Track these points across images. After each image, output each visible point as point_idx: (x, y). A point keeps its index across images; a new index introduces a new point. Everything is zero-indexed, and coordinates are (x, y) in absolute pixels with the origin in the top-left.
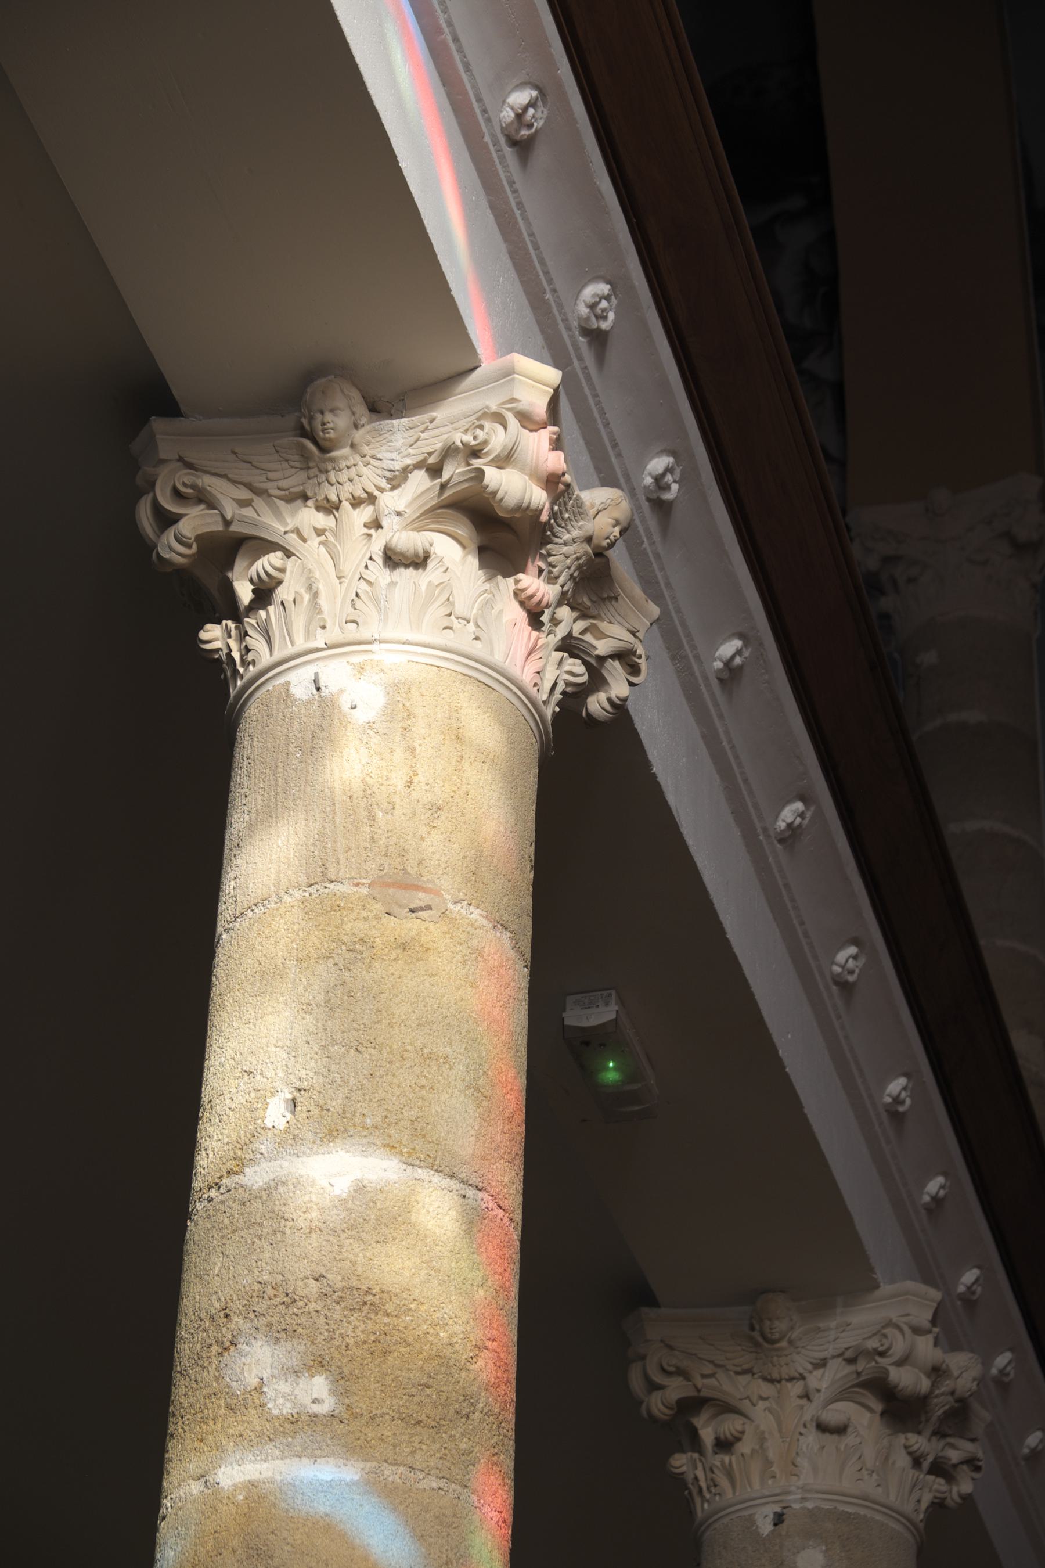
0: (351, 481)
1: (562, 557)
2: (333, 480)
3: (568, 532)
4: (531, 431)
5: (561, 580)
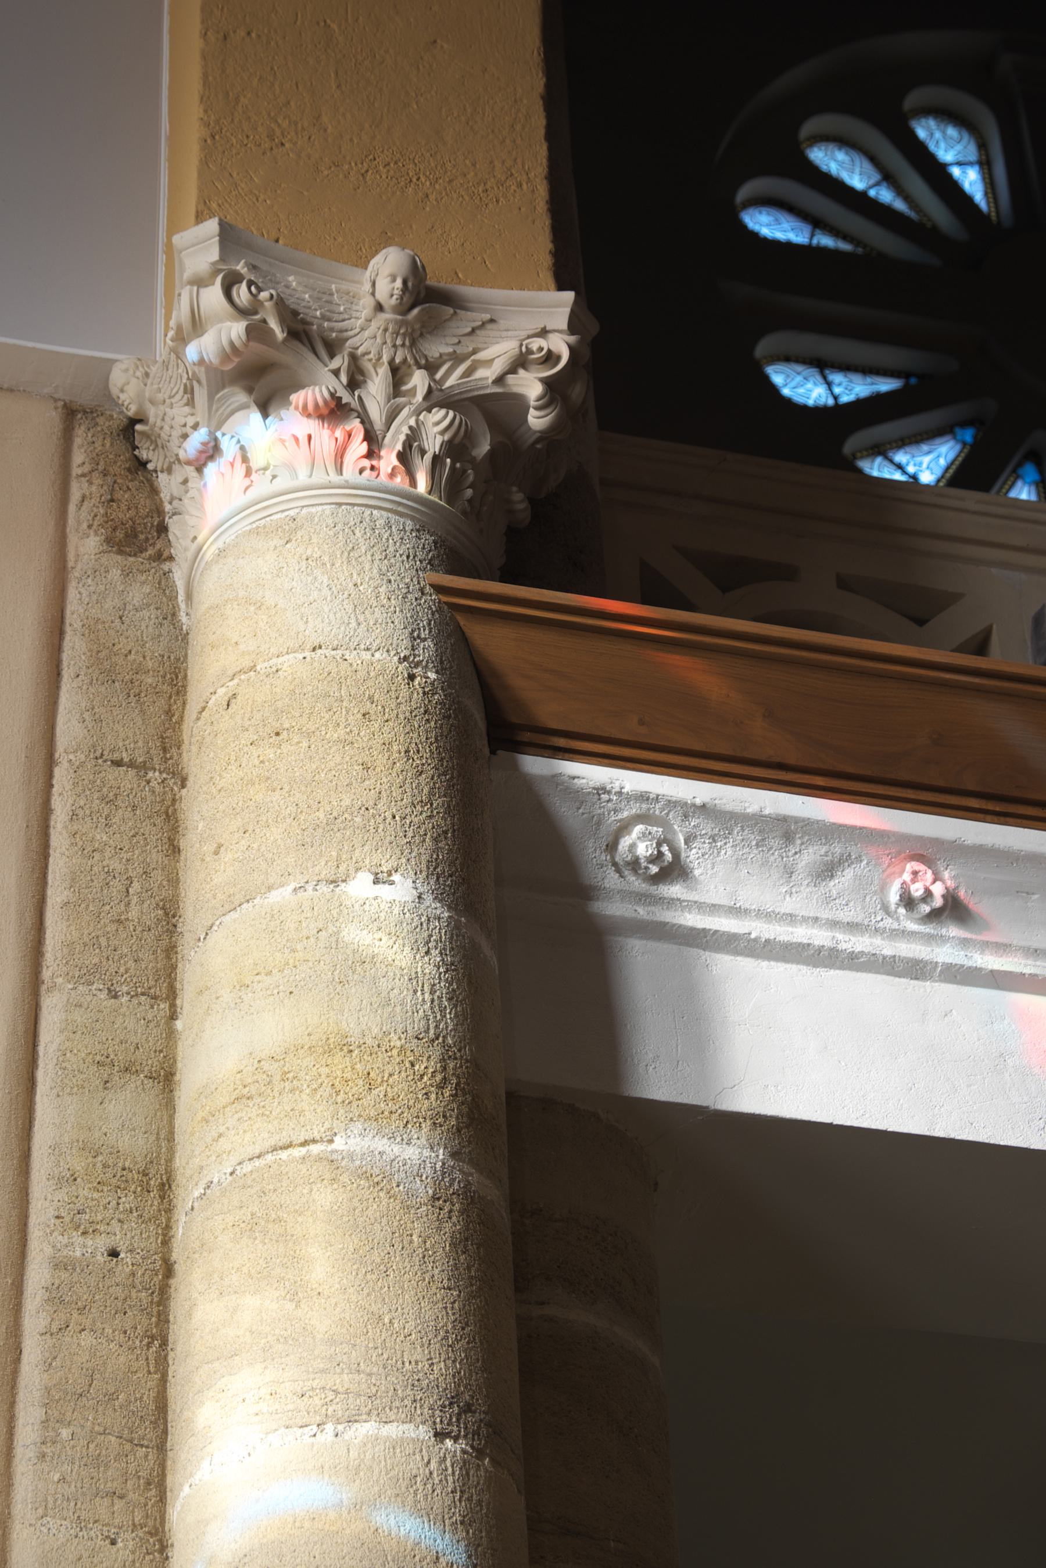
3: (357, 318)
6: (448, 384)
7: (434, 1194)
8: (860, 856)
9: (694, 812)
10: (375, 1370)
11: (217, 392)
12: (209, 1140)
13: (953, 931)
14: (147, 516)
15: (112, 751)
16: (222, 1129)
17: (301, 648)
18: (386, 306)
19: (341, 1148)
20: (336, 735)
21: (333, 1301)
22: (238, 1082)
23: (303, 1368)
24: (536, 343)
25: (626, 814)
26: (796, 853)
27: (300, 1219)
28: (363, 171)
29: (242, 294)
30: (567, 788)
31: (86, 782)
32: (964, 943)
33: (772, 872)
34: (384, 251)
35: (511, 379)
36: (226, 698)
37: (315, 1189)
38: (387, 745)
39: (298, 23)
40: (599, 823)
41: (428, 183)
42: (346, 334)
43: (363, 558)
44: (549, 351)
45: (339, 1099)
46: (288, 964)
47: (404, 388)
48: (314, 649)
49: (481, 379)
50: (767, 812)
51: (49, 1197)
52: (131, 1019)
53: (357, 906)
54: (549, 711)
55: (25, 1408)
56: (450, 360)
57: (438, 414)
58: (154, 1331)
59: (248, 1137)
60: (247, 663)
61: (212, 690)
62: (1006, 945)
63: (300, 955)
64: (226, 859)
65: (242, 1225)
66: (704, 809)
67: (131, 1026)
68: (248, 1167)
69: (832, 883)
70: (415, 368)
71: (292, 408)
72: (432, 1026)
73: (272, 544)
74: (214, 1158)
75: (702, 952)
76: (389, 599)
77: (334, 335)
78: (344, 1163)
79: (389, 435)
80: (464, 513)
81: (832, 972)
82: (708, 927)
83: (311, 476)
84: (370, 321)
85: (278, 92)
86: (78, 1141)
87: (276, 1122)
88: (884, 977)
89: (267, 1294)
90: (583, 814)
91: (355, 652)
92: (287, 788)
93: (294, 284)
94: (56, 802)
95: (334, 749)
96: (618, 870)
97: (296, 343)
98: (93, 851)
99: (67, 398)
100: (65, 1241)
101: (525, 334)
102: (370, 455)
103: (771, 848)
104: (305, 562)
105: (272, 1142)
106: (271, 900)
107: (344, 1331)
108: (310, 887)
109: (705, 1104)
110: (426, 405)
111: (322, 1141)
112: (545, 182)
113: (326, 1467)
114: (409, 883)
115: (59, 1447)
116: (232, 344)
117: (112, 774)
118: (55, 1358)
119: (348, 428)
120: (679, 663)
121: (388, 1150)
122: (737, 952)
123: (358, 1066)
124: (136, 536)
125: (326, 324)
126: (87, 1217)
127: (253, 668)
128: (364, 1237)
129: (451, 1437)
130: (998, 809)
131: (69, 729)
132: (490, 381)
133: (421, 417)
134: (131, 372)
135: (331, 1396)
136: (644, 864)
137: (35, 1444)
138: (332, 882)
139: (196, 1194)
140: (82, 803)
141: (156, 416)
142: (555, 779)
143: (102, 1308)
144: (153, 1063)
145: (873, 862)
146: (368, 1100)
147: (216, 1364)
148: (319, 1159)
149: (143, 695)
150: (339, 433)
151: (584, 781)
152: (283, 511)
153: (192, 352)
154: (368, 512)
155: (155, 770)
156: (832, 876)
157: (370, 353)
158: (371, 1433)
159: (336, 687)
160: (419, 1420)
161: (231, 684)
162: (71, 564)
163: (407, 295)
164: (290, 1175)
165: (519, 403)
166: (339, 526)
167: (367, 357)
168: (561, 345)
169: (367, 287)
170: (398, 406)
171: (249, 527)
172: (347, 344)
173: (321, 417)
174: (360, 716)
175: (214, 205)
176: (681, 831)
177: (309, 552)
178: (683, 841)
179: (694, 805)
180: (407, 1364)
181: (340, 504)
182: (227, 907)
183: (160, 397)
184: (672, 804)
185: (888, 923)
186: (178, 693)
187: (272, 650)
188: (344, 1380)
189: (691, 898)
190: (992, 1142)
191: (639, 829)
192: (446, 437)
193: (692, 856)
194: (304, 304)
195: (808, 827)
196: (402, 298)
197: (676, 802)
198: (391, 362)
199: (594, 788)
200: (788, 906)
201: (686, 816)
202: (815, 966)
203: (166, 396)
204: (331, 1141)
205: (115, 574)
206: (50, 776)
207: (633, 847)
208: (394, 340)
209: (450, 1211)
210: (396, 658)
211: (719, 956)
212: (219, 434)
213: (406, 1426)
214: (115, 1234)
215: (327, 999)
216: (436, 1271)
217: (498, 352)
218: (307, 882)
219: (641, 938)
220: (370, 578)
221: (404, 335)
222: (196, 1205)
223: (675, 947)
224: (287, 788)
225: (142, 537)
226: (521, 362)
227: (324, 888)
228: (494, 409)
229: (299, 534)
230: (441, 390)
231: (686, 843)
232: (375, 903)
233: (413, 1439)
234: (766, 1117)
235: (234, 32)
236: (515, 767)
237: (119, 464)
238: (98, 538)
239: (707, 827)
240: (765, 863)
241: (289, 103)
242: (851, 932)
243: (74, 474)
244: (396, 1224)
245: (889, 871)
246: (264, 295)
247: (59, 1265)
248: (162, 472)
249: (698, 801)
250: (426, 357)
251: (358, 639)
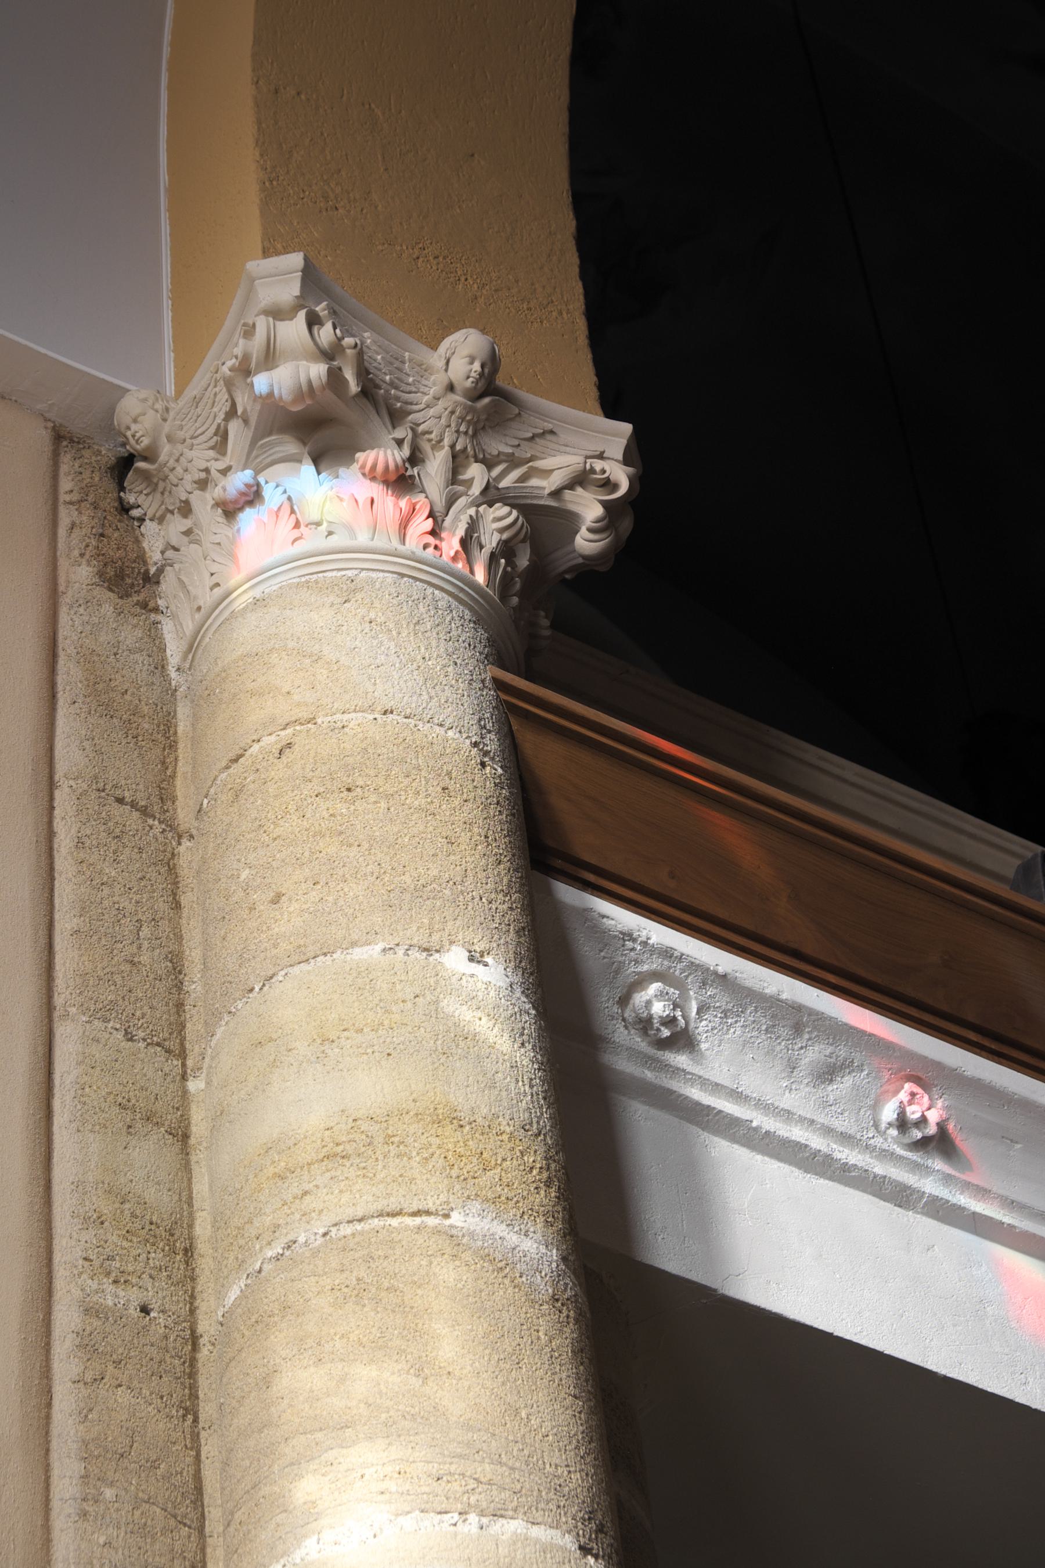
0: (186, 470)
1: (433, 421)
2: (175, 481)
3: (424, 394)
4: (291, 319)
5: (446, 442)
7: (554, 1295)
8: (862, 1065)
9: (713, 981)
10: (518, 1465)
11: (263, 437)
12: (289, 1198)
13: (938, 1164)
14: (135, 561)
15: (115, 786)
16: (307, 1187)
17: (371, 709)
18: (458, 387)
19: (460, 1224)
20: (417, 803)
21: (466, 1384)
22: (327, 1139)
23: (437, 1450)
24: (598, 465)
25: (646, 968)
26: (802, 1048)
27: (419, 1292)
28: (415, 256)
29: (326, 334)
30: (595, 926)
31: (90, 811)
32: (947, 1179)
33: (776, 1063)
34: (464, 331)
36: (279, 747)
37: (435, 1263)
38: (468, 824)
39: (345, 98)
40: (617, 972)
41: (475, 286)
42: (410, 407)
43: (429, 634)
45: (454, 1172)
46: (382, 1024)
47: (461, 477)
48: (385, 713)
49: (537, 488)
50: (784, 996)
51: (75, 1236)
52: (150, 1067)
53: (454, 980)
54: (585, 843)
55: (59, 1459)
56: (506, 461)
58: (188, 1403)
59: (345, 1198)
60: (305, 715)
61: (255, 737)
62: (985, 1190)
63: (396, 1017)
64: (291, 909)
65: (346, 1290)
66: (723, 979)
67: (150, 1074)
68: (347, 1230)
69: (830, 1088)
70: (473, 460)
71: (355, 466)
72: (535, 1120)
73: (332, 598)
74: (297, 1216)
75: (701, 1132)
76: (457, 681)
77: (399, 405)
78: (465, 1241)
81: (822, 1181)
82: (713, 1105)
83: (372, 539)
84: (439, 399)
85: (329, 158)
86: (103, 1183)
87: (381, 1186)
88: (870, 1197)
89: (385, 1365)
90: (604, 958)
91: (429, 725)
92: (366, 845)
93: (369, 341)
94: (59, 825)
95: (415, 816)
96: (626, 1027)
97: (365, 400)
98: (103, 884)
99: (59, 421)
100: (95, 1286)
103: (779, 1037)
104: (368, 624)
105: (379, 1206)
106: (355, 957)
107: (481, 1417)
108: (401, 952)
109: (713, 1286)
110: (481, 500)
111: (437, 1214)
112: (583, 317)
113: (474, 1560)
114: (501, 968)
115: (102, 1507)
116: (310, 383)
117: (117, 810)
118: (91, 1410)
120: (719, 821)
121: (508, 1237)
122: (734, 1139)
123: (471, 1143)
124: (123, 579)
125: (393, 392)
126: (118, 1265)
127: (312, 720)
128: (493, 1322)
129: (593, 1555)
130: (993, 1047)
131: (69, 755)
132: (547, 491)
133: (481, 509)
134: (150, 403)
135: (472, 1484)
136: (656, 1025)
137: (75, 1499)
138: (426, 950)
139: (270, 1253)
140: (88, 832)
141: (171, 455)
142: (586, 914)
143: (139, 1366)
144: (172, 1118)
145: (873, 1075)
146: (485, 1179)
147: (319, 1435)
148: (437, 1231)
149: (140, 738)
150: (403, 503)
151: (613, 922)
152: (339, 570)
153: (261, 382)
154: (430, 590)
155: (155, 818)
156: (831, 1080)
157: (431, 432)
158: (519, 1531)
159: (412, 755)
160: (564, 1527)
161: (282, 733)
162: (61, 588)
164: (404, 1243)
165: (569, 521)
166: (402, 597)
167: (427, 436)
169: (441, 364)
170: (455, 493)
171: (298, 580)
172: (410, 417)
173: (386, 483)
174: (439, 789)
175: (279, 246)
176: (696, 998)
177: (372, 615)
178: (695, 1010)
179: (715, 973)
180: (548, 1466)
181: (402, 575)
182: (296, 958)
183: (181, 434)
184: (695, 967)
185: (878, 1142)
186: (171, 747)
187: (336, 705)
188: (486, 1470)
189: (696, 1071)
190: (980, 1386)
191: (654, 988)
192: (505, 536)
193: (702, 1028)
194: (375, 364)
195: (820, 1023)
196: (477, 382)
197: (698, 965)
198: (452, 447)
199: (621, 933)
200: (787, 1101)
201: (704, 983)
202: (806, 1171)
204: (447, 1216)
205: (108, 609)
206: (51, 798)
207: (649, 1003)
208: (459, 425)
209: (568, 1317)
210: (468, 742)
211: (716, 1139)
213: (553, 1532)
214: (147, 1290)
215: (430, 1067)
216: (564, 1375)
217: (558, 465)
218: (398, 945)
219: (645, 1103)
220: (438, 656)
221: (469, 422)
222: (267, 1267)
223: (676, 1120)
224: (366, 845)
225: (129, 581)
226: (581, 479)
227: (415, 954)
228: (542, 523)
229: (359, 596)
230: (498, 489)
231: (698, 1013)
232: (471, 980)
233: (561, 1547)
234: (770, 1312)
235: (285, 88)
236: (549, 892)
237: (108, 500)
238: (91, 569)
239: (723, 1000)
240: (770, 1052)
241: (340, 171)
242: (842, 1144)
243: (61, 500)
244: (523, 1316)
245: (885, 1088)
247: (90, 1311)
248: (151, 520)
249: (721, 970)
250: (484, 451)
251: (431, 712)
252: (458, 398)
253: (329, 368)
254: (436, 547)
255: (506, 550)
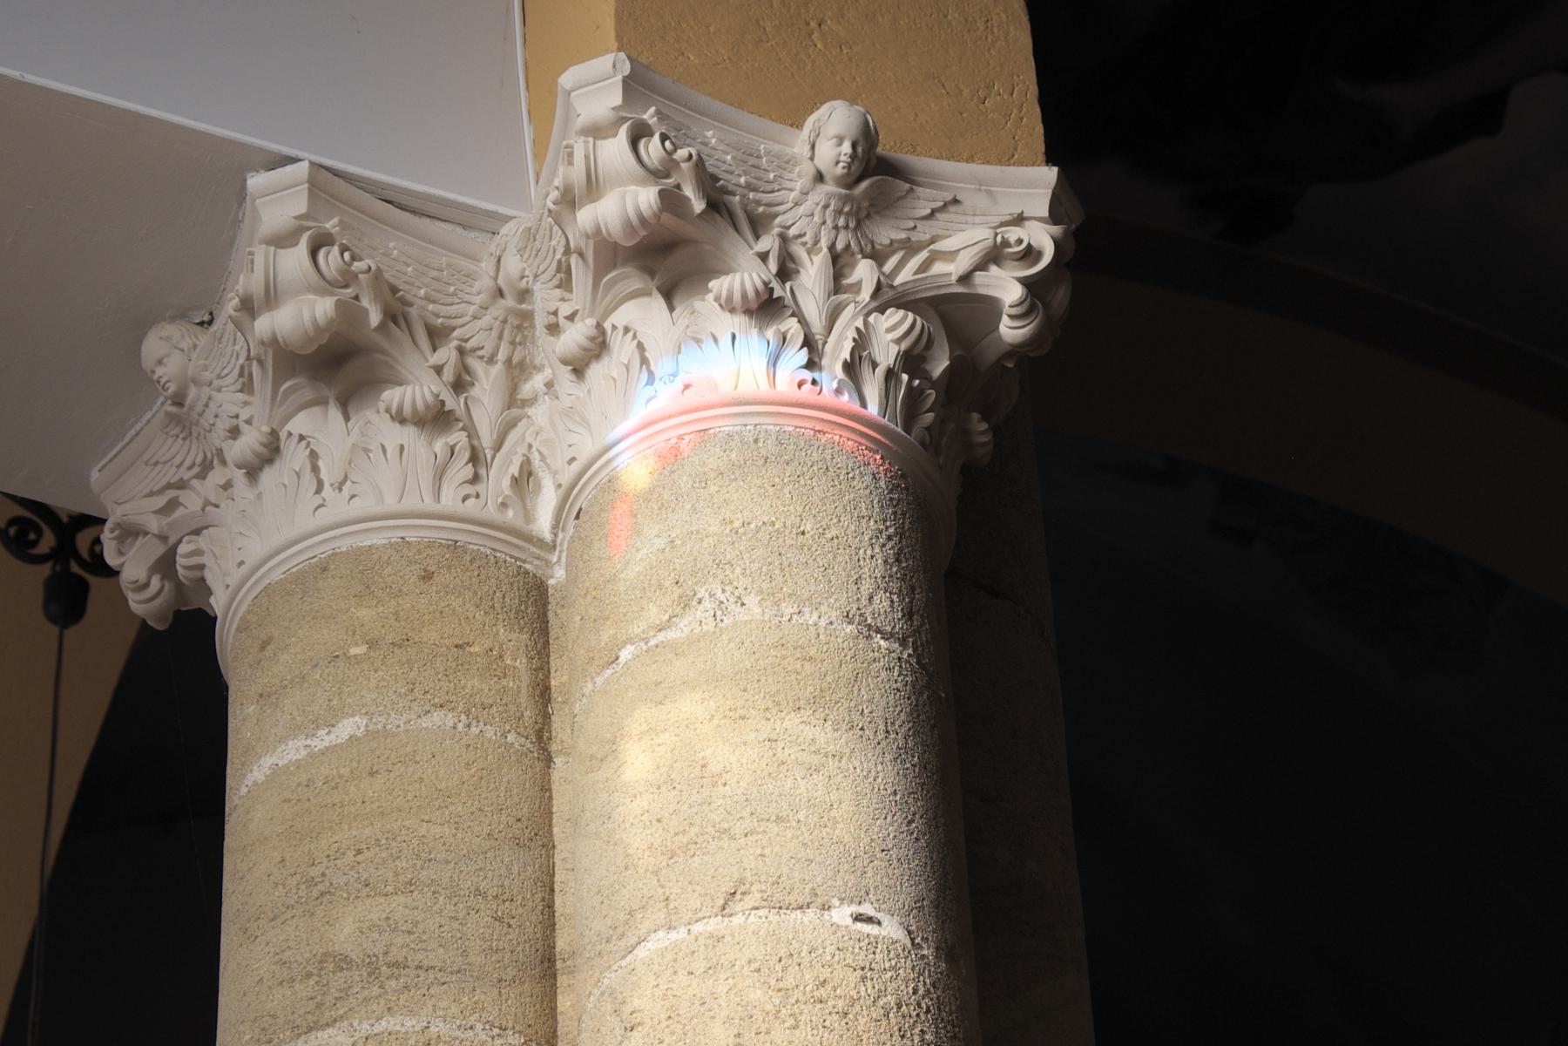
1: (805, 221)
3: (791, 190)
6: (898, 281)
24: (1013, 234)
29: (653, 149)
35: (979, 277)
44: (1029, 245)
47: (845, 282)
57: (894, 316)
71: (710, 297)
77: (761, 209)
79: (831, 340)
80: (923, 444)
101: (997, 221)
102: (811, 365)
119: (783, 327)
132: (954, 278)
133: (871, 319)
153: (586, 216)
163: (856, 163)
165: (990, 307)
168: (1043, 238)
169: (805, 150)
172: (778, 220)
173: (748, 312)
183: (207, 375)
192: (904, 346)
196: (849, 167)
198: (832, 248)
203: (213, 376)
212: (607, 325)
217: (961, 244)
226: (994, 256)
228: (953, 314)
230: (892, 287)
246: (682, 153)
250: (872, 243)
252: (829, 188)
253: (661, 192)
254: (814, 382)
255: (912, 360)
